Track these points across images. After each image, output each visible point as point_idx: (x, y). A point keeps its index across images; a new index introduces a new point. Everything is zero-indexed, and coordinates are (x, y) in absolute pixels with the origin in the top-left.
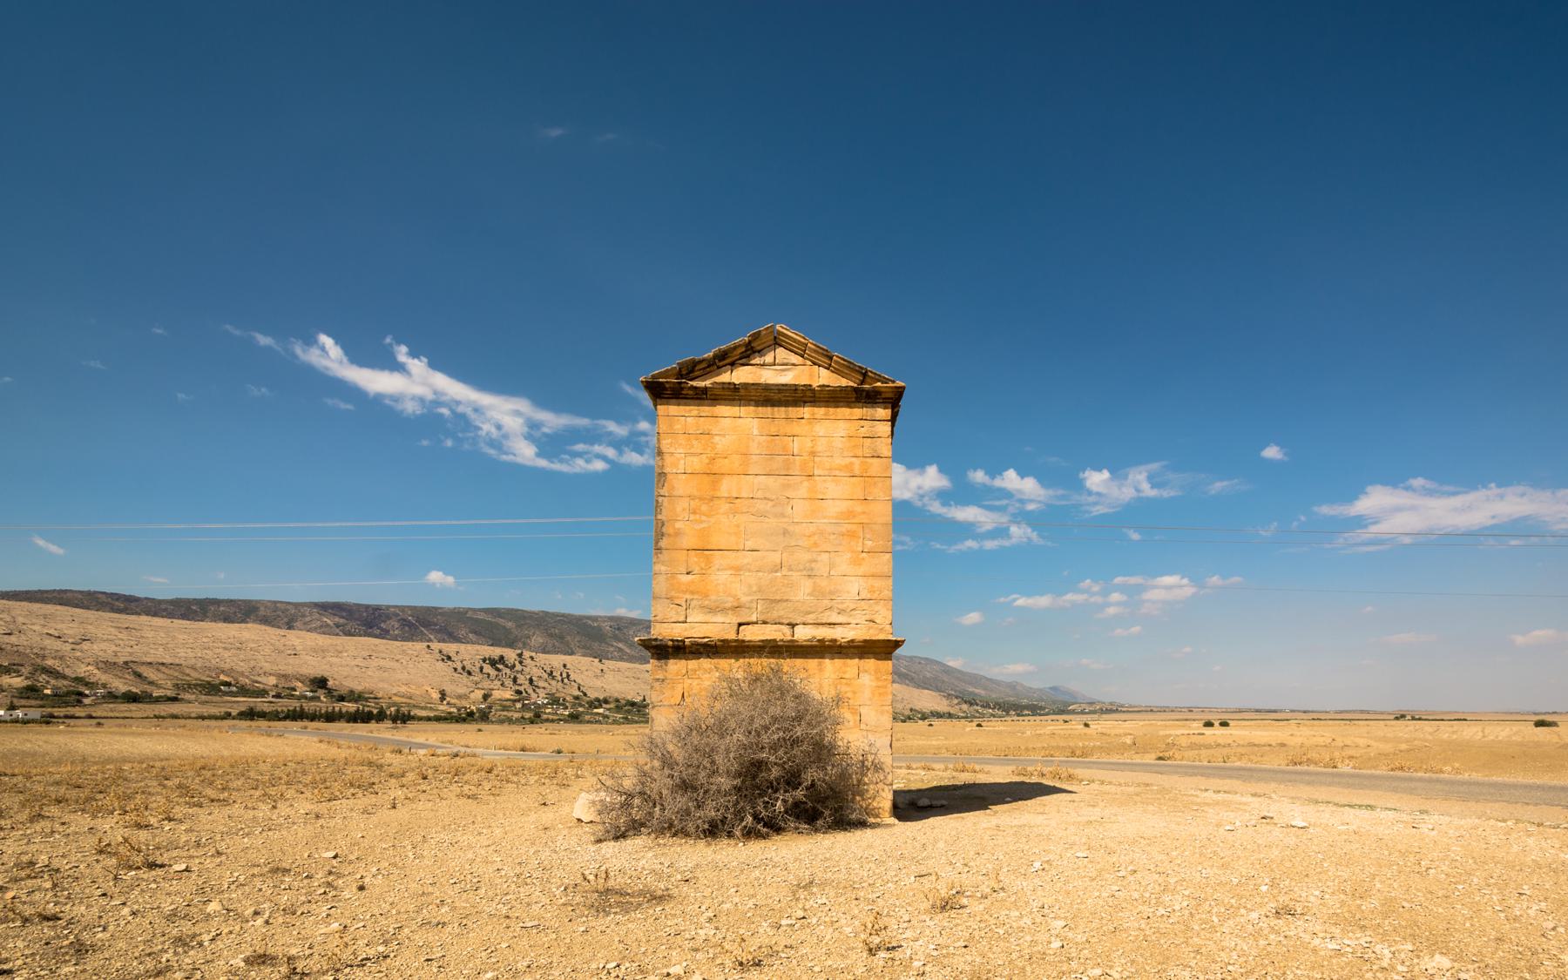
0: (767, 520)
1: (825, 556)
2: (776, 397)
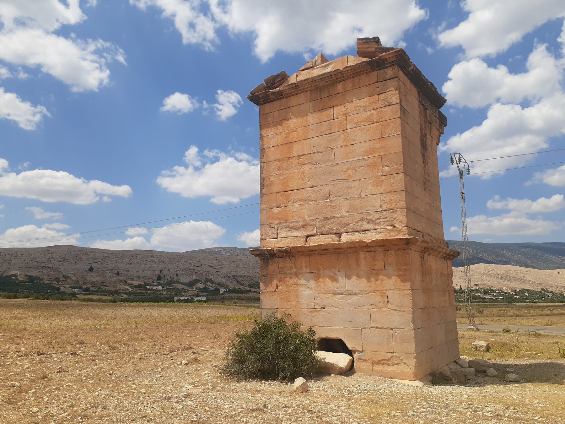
0: (320, 166)
1: (356, 184)
2: (321, 84)
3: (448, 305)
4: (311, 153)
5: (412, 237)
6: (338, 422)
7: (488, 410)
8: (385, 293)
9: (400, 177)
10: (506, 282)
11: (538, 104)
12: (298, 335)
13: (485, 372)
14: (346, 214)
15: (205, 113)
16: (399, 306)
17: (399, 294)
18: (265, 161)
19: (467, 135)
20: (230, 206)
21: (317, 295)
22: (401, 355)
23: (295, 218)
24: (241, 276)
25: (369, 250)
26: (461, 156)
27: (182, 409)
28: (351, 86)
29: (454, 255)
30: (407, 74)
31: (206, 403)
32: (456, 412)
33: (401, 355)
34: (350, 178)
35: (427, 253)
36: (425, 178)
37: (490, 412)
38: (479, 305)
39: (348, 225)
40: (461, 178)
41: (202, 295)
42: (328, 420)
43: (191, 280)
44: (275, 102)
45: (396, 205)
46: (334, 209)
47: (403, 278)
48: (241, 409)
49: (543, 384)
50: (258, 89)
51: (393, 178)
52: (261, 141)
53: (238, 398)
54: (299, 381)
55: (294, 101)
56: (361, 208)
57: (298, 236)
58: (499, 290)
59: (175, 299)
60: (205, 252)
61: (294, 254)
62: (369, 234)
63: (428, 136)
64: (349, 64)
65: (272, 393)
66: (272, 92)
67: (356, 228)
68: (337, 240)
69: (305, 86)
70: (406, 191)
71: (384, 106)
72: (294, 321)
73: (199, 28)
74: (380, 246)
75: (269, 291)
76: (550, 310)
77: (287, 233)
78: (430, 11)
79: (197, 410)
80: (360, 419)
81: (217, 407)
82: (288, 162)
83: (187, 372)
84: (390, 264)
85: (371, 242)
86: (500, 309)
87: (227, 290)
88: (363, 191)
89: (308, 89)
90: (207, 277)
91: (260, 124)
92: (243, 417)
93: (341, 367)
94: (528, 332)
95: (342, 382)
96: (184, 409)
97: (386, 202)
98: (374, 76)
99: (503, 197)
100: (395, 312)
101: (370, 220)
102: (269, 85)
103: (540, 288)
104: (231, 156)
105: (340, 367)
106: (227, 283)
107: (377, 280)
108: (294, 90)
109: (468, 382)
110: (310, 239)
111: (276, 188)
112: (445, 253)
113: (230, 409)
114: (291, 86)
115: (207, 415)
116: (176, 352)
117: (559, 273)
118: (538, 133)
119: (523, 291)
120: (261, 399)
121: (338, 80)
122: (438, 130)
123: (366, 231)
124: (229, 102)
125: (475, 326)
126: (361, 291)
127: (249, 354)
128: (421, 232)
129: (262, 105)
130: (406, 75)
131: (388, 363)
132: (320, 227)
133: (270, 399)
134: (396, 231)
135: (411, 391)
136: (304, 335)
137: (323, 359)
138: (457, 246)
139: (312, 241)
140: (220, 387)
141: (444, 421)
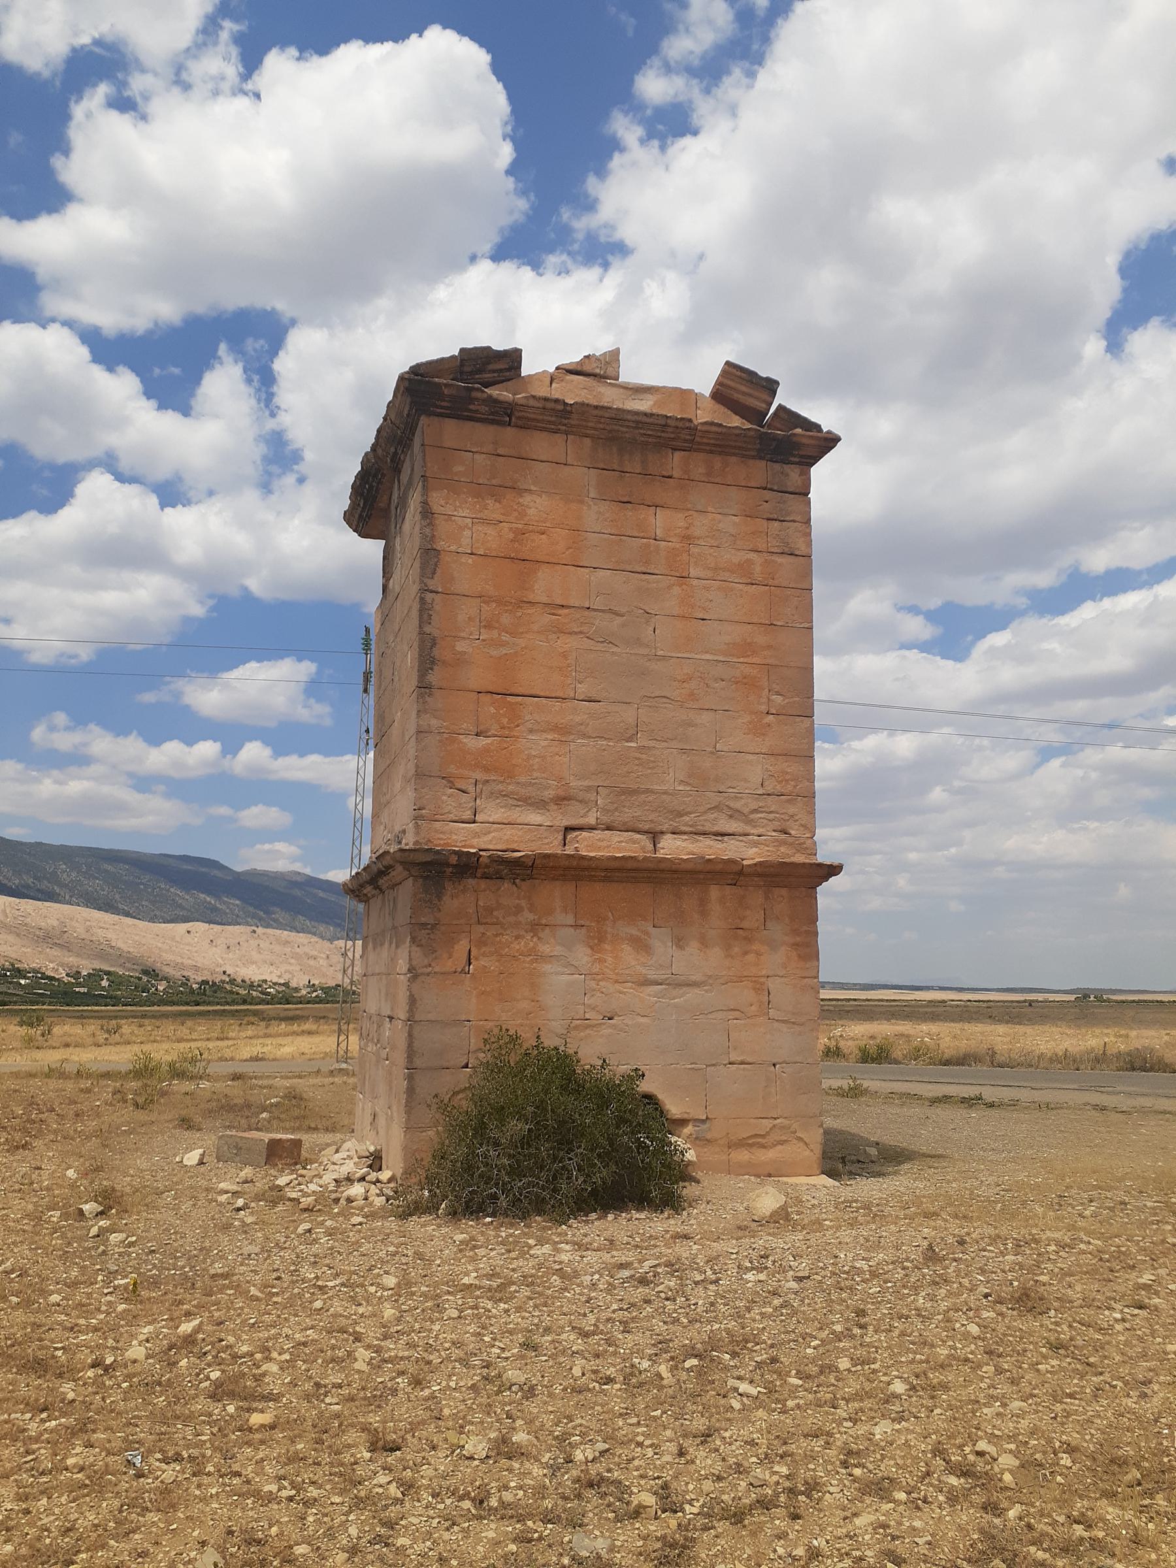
0: (615, 649)
1: (706, 717)
8: (762, 984)
14: (680, 788)
16: (794, 1014)
21: (593, 984)
23: (535, 774)
28: (704, 471)
39: (681, 816)
45: (795, 787)
46: (649, 771)
52: (424, 523)
55: (541, 445)
58: (35, 971)
66: (490, 396)
67: (703, 826)
71: (778, 551)
75: (443, 970)
77: (509, 813)
89: (588, 432)
98: (760, 470)
99: (79, 721)
100: (784, 1028)
107: (746, 953)
110: (577, 836)
111: (476, 677)
114: (550, 405)
117: (189, 932)
118: (186, 574)
119: (96, 975)
126: (710, 977)
129: (436, 419)
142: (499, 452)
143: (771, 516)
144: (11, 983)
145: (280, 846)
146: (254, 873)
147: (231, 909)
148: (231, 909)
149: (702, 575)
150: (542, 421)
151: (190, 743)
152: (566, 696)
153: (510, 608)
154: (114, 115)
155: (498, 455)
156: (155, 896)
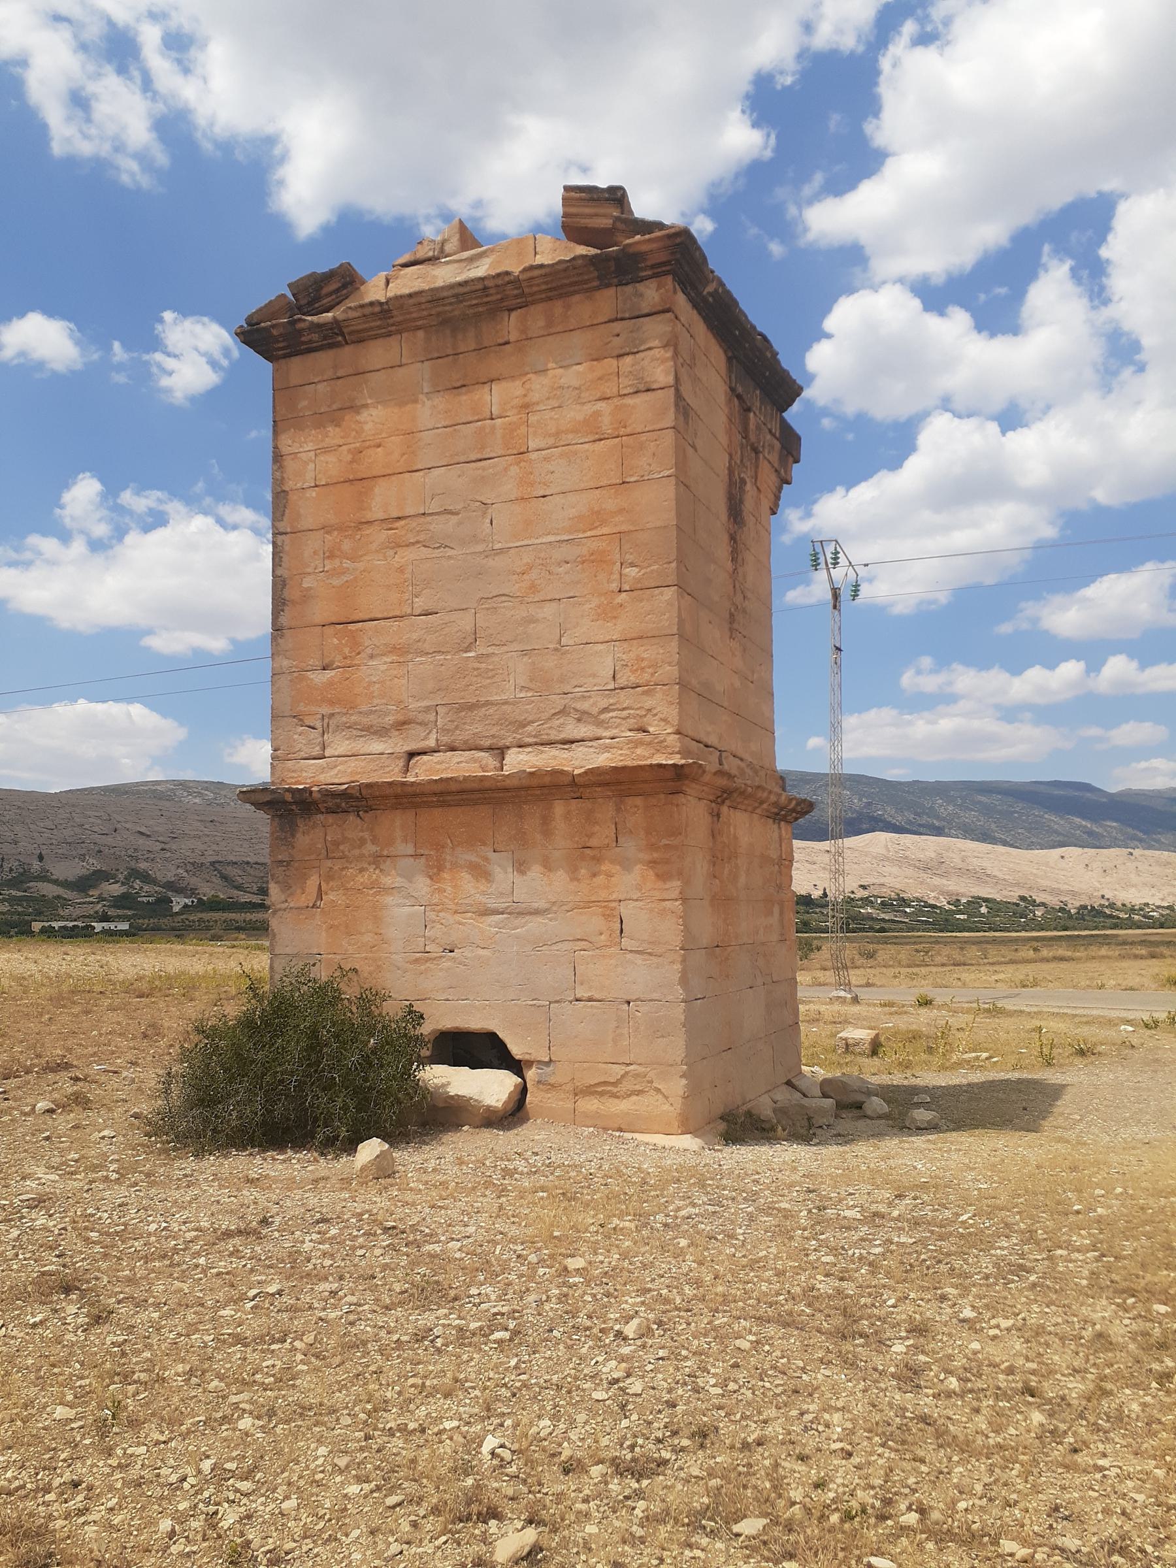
0: (450, 552)
1: (549, 610)
3: (775, 937)
4: (424, 514)
5: (691, 761)
6: (464, 1255)
7: (852, 1203)
8: (613, 909)
9: (667, 598)
10: (937, 881)
11: (1040, 419)
12: (375, 1025)
13: (859, 1106)
15: (120, 378)
17: (651, 911)
18: (289, 530)
19: (864, 492)
20: (200, 661)
21: (432, 915)
22: (648, 1069)
23: (376, 701)
24: (236, 863)
25: (578, 795)
26: (839, 549)
27: (17, 1239)
29: (799, 809)
30: (699, 303)
31: (92, 1219)
32: (775, 1212)
33: (648, 1069)
34: (533, 593)
35: (728, 802)
36: (734, 604)
37: (857, 1209)
38: (867, 937)
39: (524, 727)
40: (835, 607)
41: (119, 916)
42: (438, 1249)
43: (85, 872)
44: (320, 353)
45: (652, 675)
46: (489, 681)
47: (663, 869)
48: (196, 1233)
49: (992, 1133)
50: (270, 311)
51: (648, 600)
52: (276, 468)
53: (190, 1202)
54: (370, 1149)
55: (378, 353)
56: (562, 680)
57: (382, 754)
59: (37, 926)
60: (127, 792)
61: (370, 803)
62: (579, 751)
63: (748, 487)
64: (539, 260)
65: (291, 1184)
66: (312, 323)
68: (492, 767)
69: (412, 313)
70: (682, 637)
71: (631, 391)
72: (366, 986)
73: (102, 109)
74: (607, 784)
75: (297, 906)
76: (1035, 950)
77: (353, 745)
78: (777, 137)
79: (63, 1240)
80: (522, 1244)
81: (123, 1230)
82: (358, 537)
83: (48, 1133)
84: (631, 831)
85: (586, 773)
86: (916, 947)
87: (193, 902)
88: (569, 632)
90: (133, 864)
91: (274, 417)
92: (197, 1254)
93: (491, 1106)
94: (975, 1005)
95: (491, 1146)
96: (24, 1240)
97: (626, 665)
98: (607, 300)
99: (943, 662)
100: (638, 959)
101: (585, 712)
102: (303, 302)
103: (1017, 894)
104: (206, 513)
105: (488, 1107)
106: (194, 881)
107: (594, 875)
108: (379, 323)
109: (814, 1134)
111: (321, 611)
112: (775, 804)
113: (164, 1233)
114: (368, 311)
115: (93, 1252)
116: (21, 1077)
117: (1062, 857)
118: (1033, 496)
119: (976, 902)
120: (255, 1203)
121: (505, 304)
122: (776, 471)
123: (572, 742)
124: (196, 349)
125: (850, 991)
127: (231, 1081)
128: (716, 749)
130: (695, 306)
131: (615, 1090)
132: (448, 730)
133: (281, 1203)
134: (649, 744)
135: (669, 1162)
136: (392, 1024)
137: (443, 1086)
138: (820, 787)
139: (424, 767)
140: (140, 1172)
141: (741, 1237)
142: (339, 375)
143: (622, 352)
144: (897, 911)
145: (1157, 763)
146: (1128, 793)
147: (1108, 833)
148: (1108, 833)
149: (542, 445)
150: (372, 329)
151: (1051, 666)
152: (403, 614)
153: (350, 532)
154: (919, 51)
155: (338, 378)
156: (1030, 823)
